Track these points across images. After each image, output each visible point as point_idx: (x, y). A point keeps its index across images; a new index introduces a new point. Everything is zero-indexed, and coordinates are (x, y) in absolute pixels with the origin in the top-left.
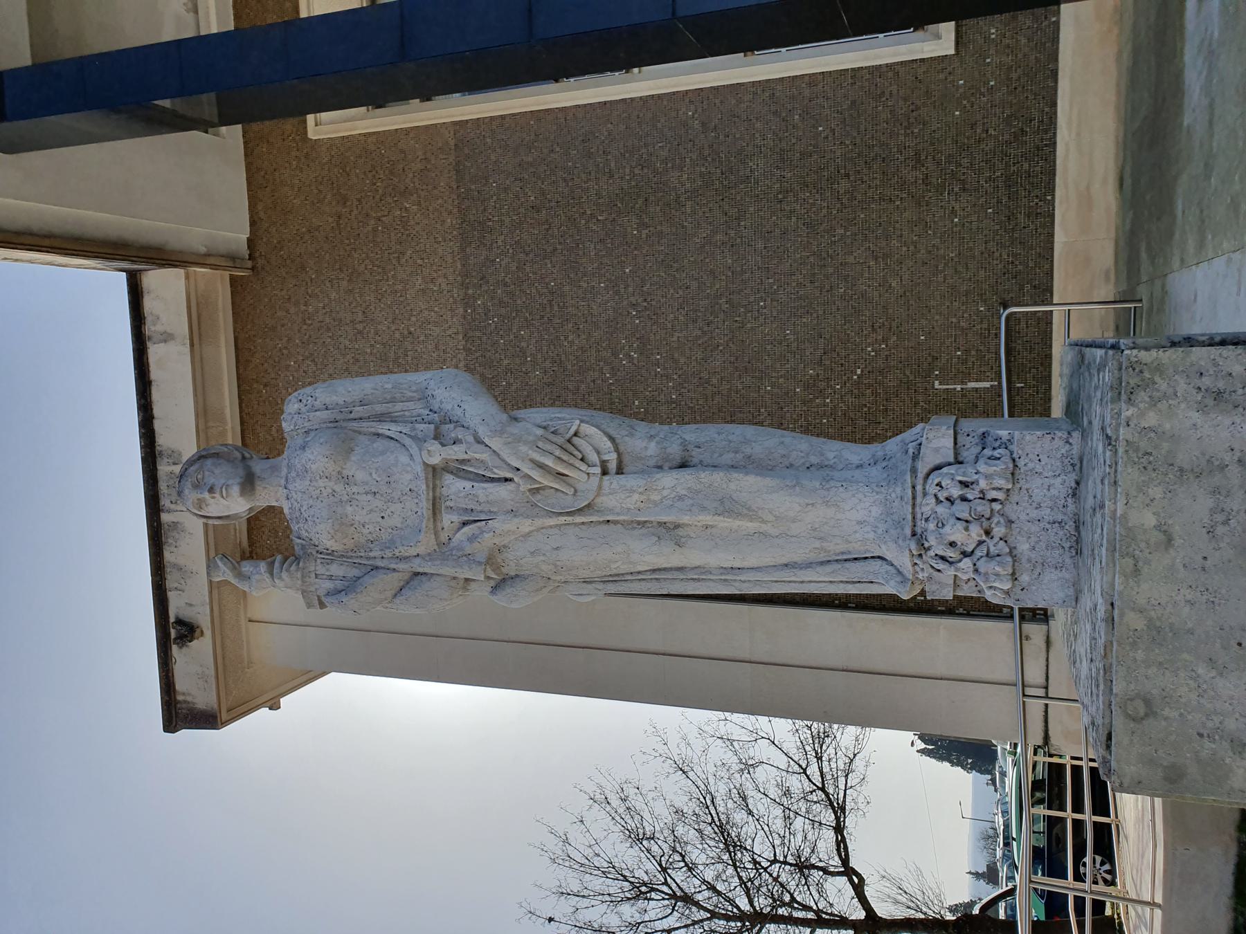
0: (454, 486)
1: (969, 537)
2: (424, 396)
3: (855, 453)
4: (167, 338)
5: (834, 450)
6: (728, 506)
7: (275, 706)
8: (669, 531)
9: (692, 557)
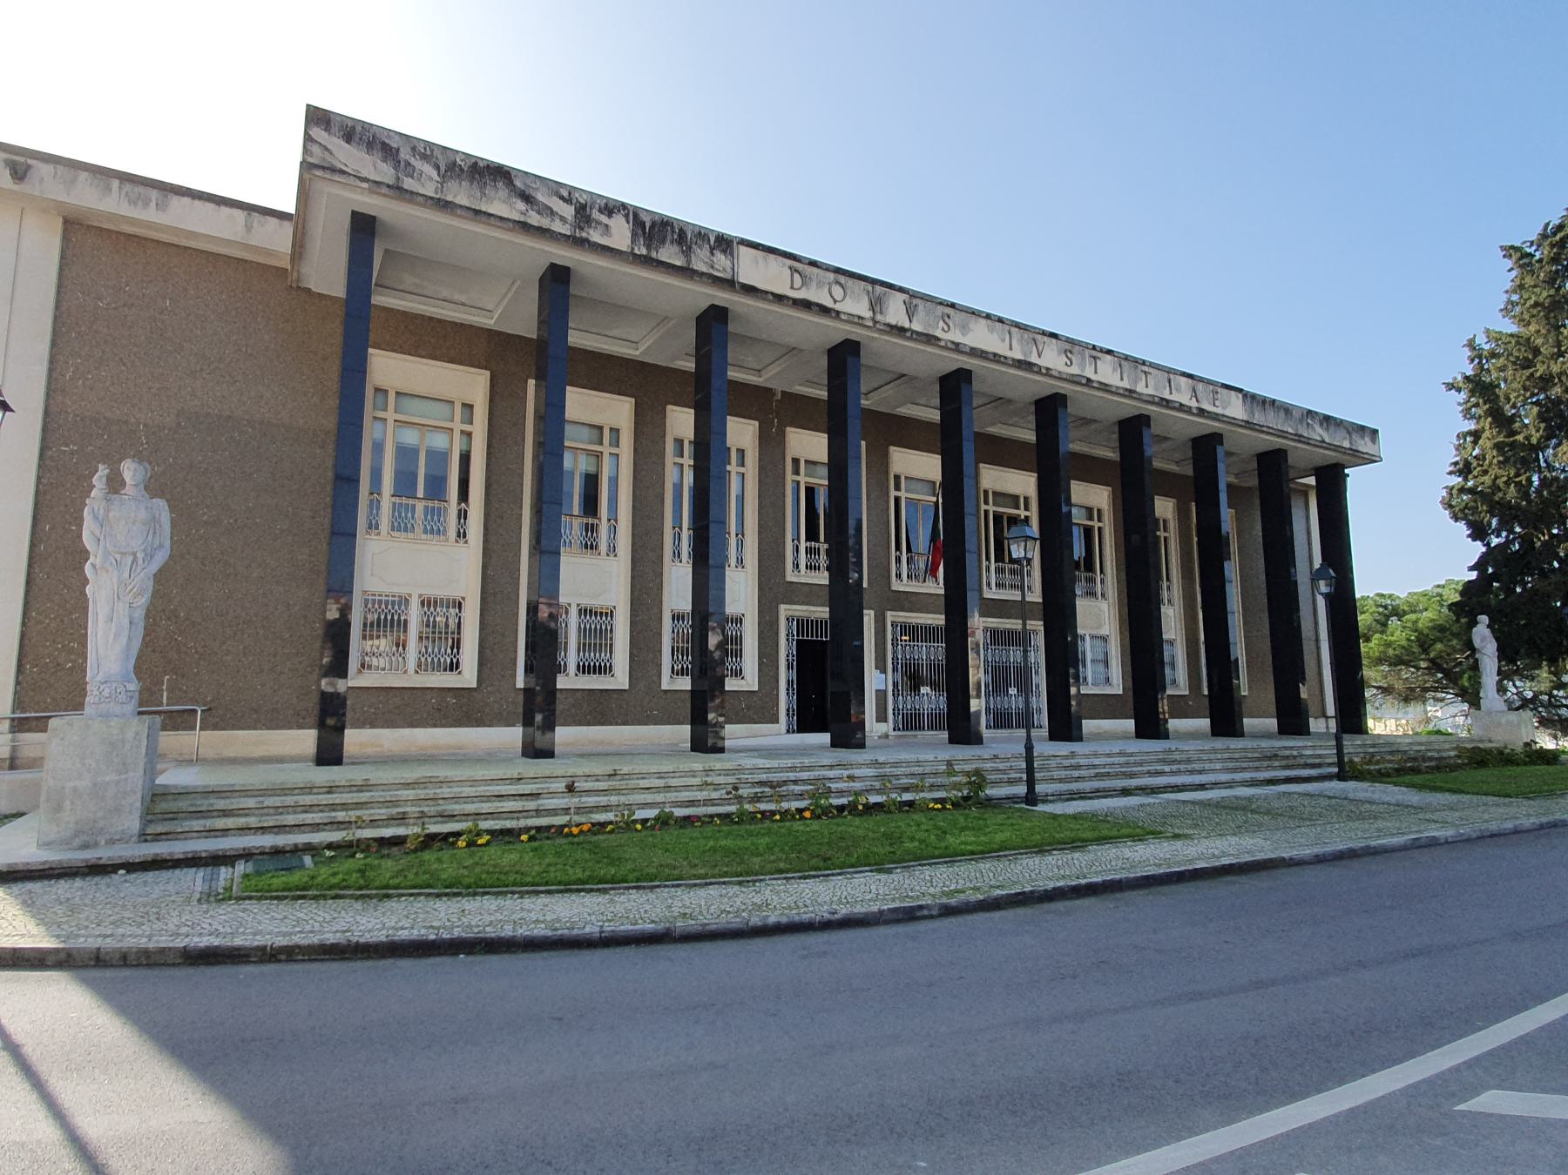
0: (130, 559)
1: (106, 693)
2: (161, 546)
4: (248, 228)
6: (117, 636)
9: (101, 624)
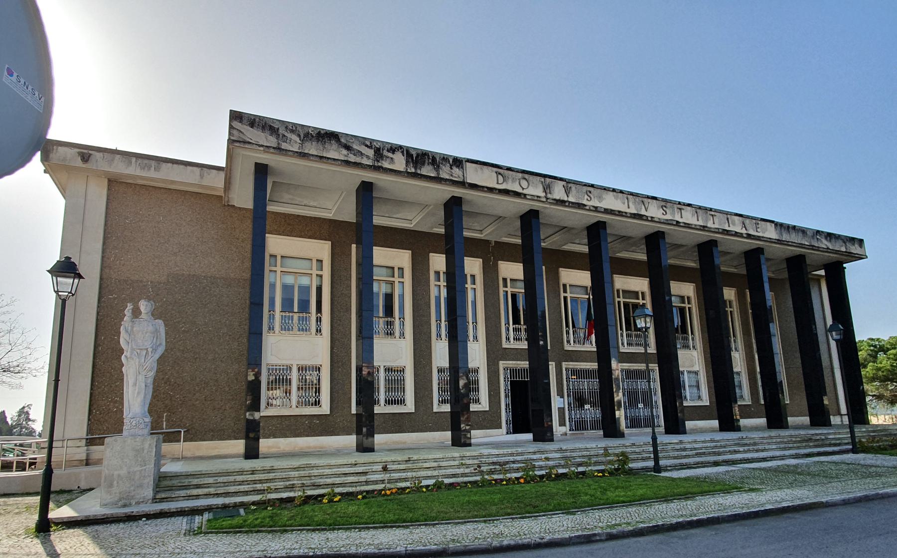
1: (134, 423)
2: (160, 344)
3: (146, 409)
4: (202, 176)
5: (147, 406)
6: (138, 393)
7: (45, 172)
8: (135, 384)
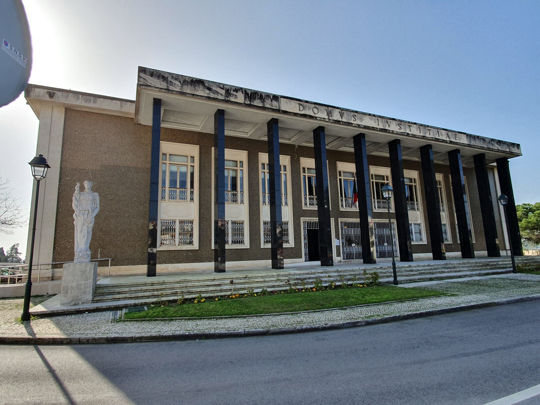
1: (80, 255)
2: (97, 207)
3: (88, 246)
4: (121, 106)
6: (83, 237)
7: (27, 103)
8: (81, 231)
